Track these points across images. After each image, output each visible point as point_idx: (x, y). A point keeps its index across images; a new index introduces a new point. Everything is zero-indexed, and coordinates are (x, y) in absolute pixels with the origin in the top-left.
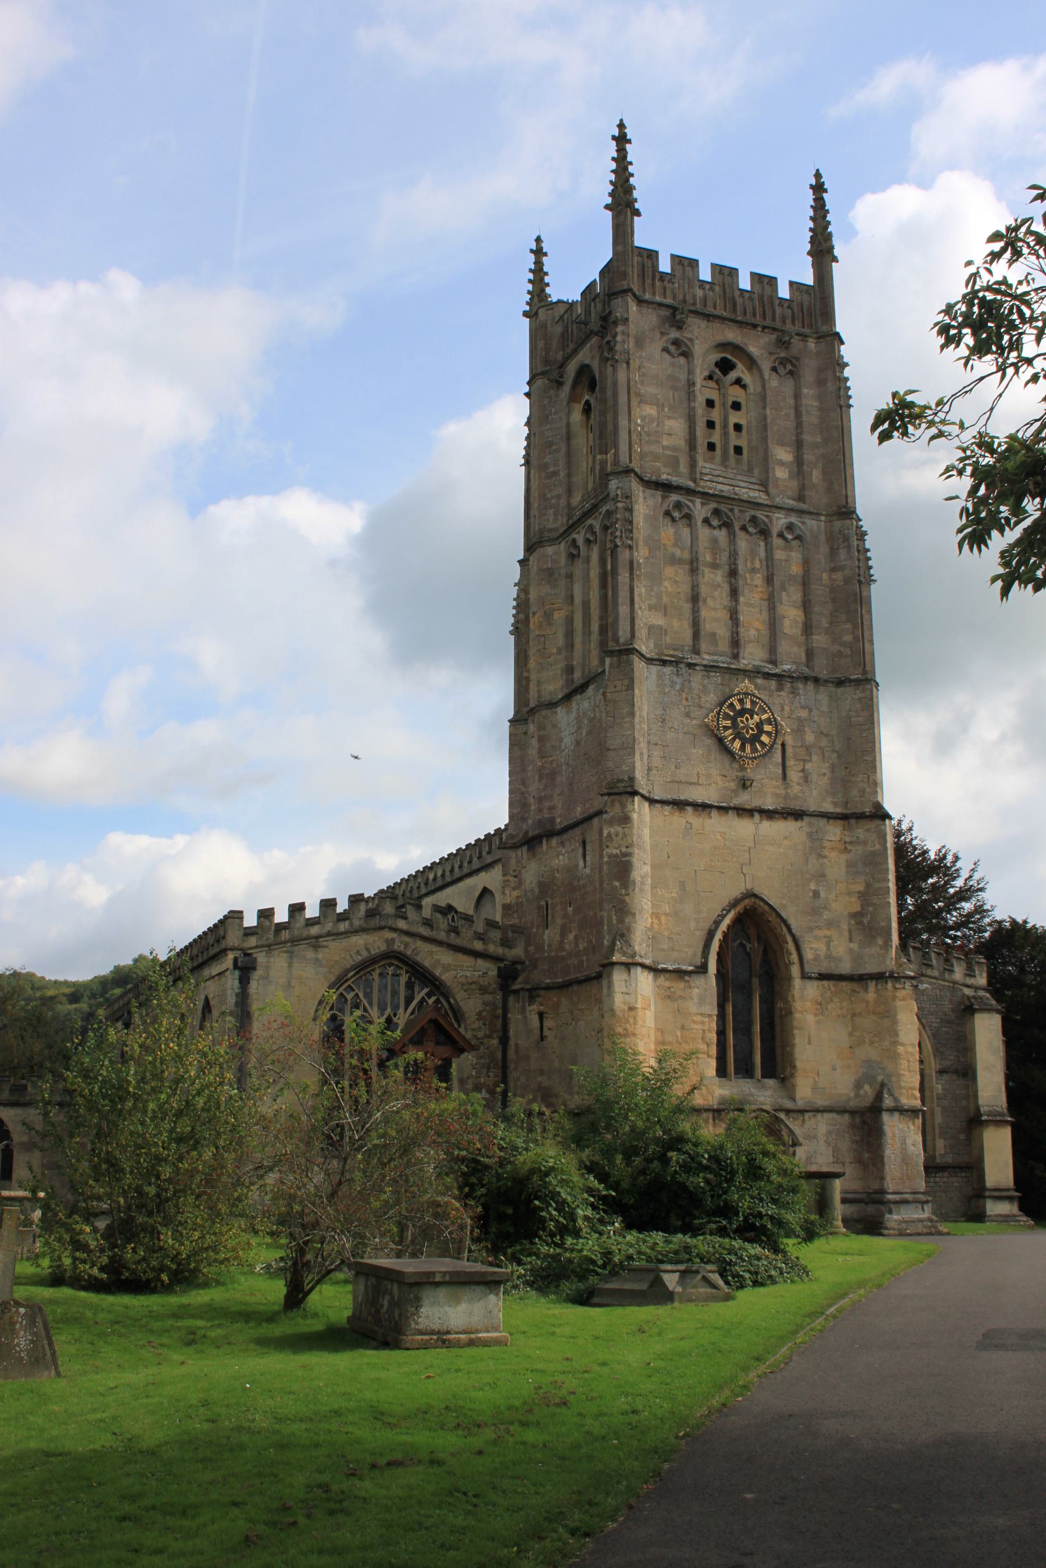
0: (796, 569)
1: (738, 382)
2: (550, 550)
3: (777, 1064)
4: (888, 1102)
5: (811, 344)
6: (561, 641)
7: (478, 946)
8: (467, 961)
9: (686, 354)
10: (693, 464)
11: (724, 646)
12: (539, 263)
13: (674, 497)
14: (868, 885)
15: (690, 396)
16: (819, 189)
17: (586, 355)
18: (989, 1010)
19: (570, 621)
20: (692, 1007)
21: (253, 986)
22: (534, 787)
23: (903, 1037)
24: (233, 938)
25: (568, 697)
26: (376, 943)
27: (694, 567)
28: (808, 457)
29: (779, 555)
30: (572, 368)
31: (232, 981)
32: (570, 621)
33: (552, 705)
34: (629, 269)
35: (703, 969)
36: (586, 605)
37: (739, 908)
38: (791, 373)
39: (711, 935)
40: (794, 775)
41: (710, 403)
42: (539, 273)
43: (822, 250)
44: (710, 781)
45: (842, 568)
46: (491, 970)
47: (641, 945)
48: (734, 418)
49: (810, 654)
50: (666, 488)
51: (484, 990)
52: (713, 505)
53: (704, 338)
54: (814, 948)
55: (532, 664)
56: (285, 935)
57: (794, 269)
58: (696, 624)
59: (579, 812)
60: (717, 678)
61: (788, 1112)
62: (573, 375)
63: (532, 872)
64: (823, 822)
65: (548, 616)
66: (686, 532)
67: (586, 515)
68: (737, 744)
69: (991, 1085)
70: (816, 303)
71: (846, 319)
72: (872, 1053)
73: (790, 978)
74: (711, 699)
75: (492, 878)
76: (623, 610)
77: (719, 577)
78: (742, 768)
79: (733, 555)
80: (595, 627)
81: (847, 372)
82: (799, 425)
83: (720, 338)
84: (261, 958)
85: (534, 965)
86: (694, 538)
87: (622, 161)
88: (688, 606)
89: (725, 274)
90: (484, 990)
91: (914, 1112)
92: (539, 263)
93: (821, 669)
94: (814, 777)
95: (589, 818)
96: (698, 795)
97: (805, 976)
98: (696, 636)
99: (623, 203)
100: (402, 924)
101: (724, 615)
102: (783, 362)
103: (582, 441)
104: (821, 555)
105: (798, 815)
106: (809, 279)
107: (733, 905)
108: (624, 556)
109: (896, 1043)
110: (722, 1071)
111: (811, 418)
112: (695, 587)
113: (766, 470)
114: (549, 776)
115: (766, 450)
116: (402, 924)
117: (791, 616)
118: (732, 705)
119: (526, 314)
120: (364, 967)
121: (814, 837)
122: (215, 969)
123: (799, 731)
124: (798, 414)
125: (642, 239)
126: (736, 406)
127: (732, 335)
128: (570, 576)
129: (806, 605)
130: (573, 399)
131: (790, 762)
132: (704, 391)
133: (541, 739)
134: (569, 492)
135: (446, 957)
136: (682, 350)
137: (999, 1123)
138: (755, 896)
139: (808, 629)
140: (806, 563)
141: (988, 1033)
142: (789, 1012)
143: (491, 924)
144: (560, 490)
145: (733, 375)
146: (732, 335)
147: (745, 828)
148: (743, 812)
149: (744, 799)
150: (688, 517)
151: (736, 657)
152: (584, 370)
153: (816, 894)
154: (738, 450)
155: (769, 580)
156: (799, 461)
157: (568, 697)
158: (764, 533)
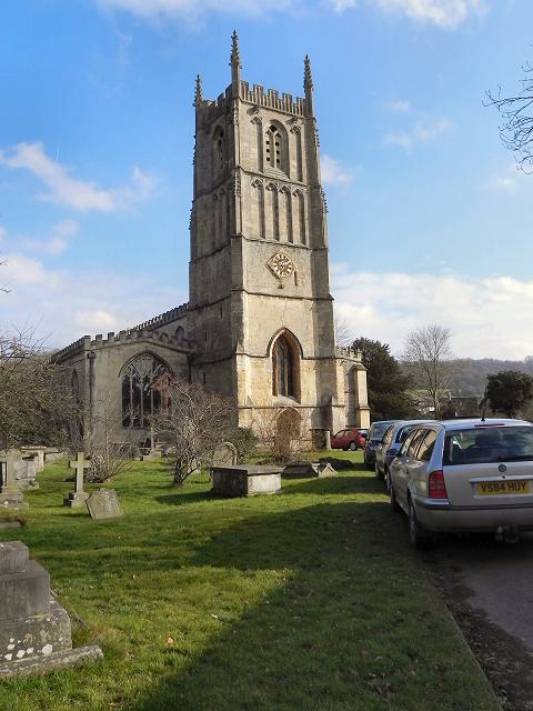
2: (205, 197)
4: (333, 403)
6: (210, 232)
7: (180, 348)
8: (176, 354)
13: (255, 178)
16: (307, 62)
17: (218, 122)
19: (214, 224)
20: (264, 369)
21: (95, 365)
22: (200, 288)
24: (87, 346)
25: (213, 254)
26: (141, 347)
30: (214, 126)
31: (87, 362)
32: (214, 224)
33: (207, 256)
35: (268, 355)
36: (220, 218)
42: (198, 88)
43: (308, 86)
44: (270, 286)
46: (184, 357)
47: (247, 349)
51: (182, 365)
55: (199, 241)
56: (106, 345)
59: (219, 297)
60: (271, 247)
63: (200, 321)
65: (205, 222)
67: (220, 184)
69: (363, 398)
72: (328, 386)
75: (182, 323)
80: (225, 227)
83: (272, 118)
84: (98, 354)
85: (201, 355)
90: (182, 365)
95: (223, 299)
96: (265, 291)
99: (235, 63)
100: (151, 340)
103: (218, 156)
105: (301, 299)
107: (278, 332)
110: (274, 394)
114: (206, 284)
116: (151, 340)
120: (138, 356)
122: (78, 358)
125: (204, 98)
127: (276, 116)
128: (213, 208)
130: (214, 139)
133: (203, 270)
134: (213, 174)
135: (167, 352)
136: (258, 122)
141: (362, 376)
142: (299, 371)
143: (183, 339)
144: (210, 174)
146: (276, 116)
147: (282, 302)
149: (281, 292)
152: (218, 127)
157: (213, 254)
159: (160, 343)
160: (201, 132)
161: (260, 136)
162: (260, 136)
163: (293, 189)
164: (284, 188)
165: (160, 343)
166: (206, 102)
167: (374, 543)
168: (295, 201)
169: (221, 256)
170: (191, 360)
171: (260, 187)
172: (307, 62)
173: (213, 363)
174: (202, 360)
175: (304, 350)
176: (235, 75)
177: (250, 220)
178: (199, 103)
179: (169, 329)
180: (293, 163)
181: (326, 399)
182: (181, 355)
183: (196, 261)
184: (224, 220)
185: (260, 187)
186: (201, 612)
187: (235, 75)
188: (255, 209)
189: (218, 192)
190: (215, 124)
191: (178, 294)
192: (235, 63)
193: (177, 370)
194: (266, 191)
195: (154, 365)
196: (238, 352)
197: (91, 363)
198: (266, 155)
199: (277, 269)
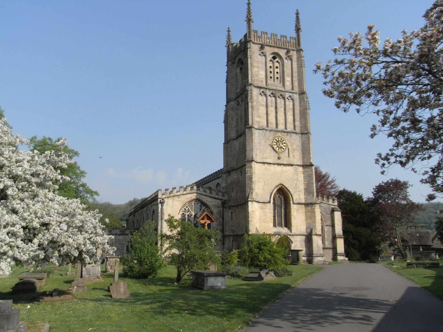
1: (277, 62)
3: (288, 224)
8: (214, 200)
13: (262, 90)
16: (297, 14)
24: (160, 196)
30: (237, 59)
37: (278, 187)
39: (272, 194)
40: (291, 156)
42: (229, 36)
43: (298, 30)
44: (271, 157)
45: (302, 106)
46: (220, 202)
48: (276, 70)
51: (218, 207)
56: (172, 195)
60: (272, 132)
61: (290, 235)
64: (298, 167)
65: (232, 118)
68: (277, 148)
69: (339, 229)
73: (290, 204)
74: (271, 138)
80: (243, 121)
84: (166, 200)
87: (298, 18)
90: (218, 207)
91: (320, 235)
96: (268, 161)
97: (293, 203)
99: (249, 21)
103: (240, 77)
105: (292, 165)
107: (277, 187)
109: (315, 219)
110: (275, 225)
118: (276, 140)
122: (155, 203)
126: (277, 67)
127: (276, 50)
131: (290, 153)
132: (269, 64)
134: (237, 88)
138: (282, 185)
141: (338, 216)
148: (278, 164)
151: (277, 128)
153: (296, 184)
154: (277, 78)
159: (204, 193)
160: (230, 63)
161: (266, 63)
162: (266, 63)
163: (287, 95)
164: (281, 95)
165: (204, 193)
166: (232, 44)
167: (34, 220)
168: (289, 104)
169: (241, 139)
170: (224, 204)
171: (265, 95)
172: (297, 14)
173: (237, 206)
174: (231, 204)
175: (294, 198)
176: (249, 27)
177: (259, 117)
178: (229, 44)
179: (212, 185)
180: (288, 79)
181: (309, 230)
182: (218, 201)
183: (227, 142)
184: (243, 116)
185: (265, 95)
186: (35, 216)
187: (249, 27)
188: (263, 110)
189: (240, 100)
190: (238, 58)
191: (216, 163)
192: (249, 21)
193: (215, 210)
194: (269, 98)
195: (201, 206)
196: (249, 199)
197: (162, 206)
198: (269, 75)
199: (277, 146)
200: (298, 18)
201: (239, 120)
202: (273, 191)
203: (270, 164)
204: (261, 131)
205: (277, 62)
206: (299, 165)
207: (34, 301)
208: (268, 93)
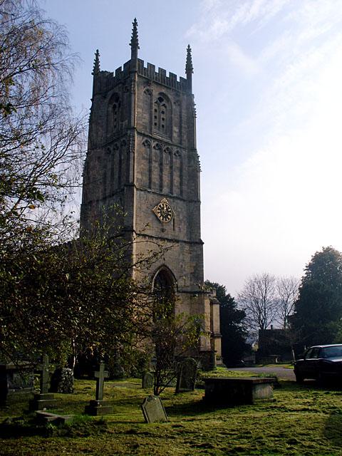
0: (178, 165)
1: (164, 105)
5: (185, 97)
9: (151, 94)
10: (151, 129)
11: (157, 187)
12: (97, 58)
13: (146, 138)
14: (197, 264)
15: (151, 107)
16: (135, 24)
18: (217, 304)
23: (206, 311)
27: (150, 162)
28: (183, 131)
29: (174, 160)
30: (110, 93)
34: (133, 65)
37: (161, 269)
38: (179, 105)
40: (177, 229)
41: (156, 110)
42: (97, 62)
43: (189, 69)
45: (192, 166)
48: (162, 116)
49: (181, 192)
50: (144, 135)
52: (156, 143)
53: (156, 92)
54: (180, 283)
57: (181, 74)
58: (150, 179)
62: (110, 96)
64: (184, 244)
66: (148, 149)
68: (161, 218)
70: (187, 83)
71: (196, 89)
76: (131, 172)
77: (157, 165)
78: (163, 226)
79: (162, 158)
81: (195, 107)
82: (181, 121)
86: (151, 152)
87: (135, 31)
88: (148, 173)
89: (163, 71)
92: (97, 58)
93: (185, 197)
94: (182, 230)
98: (150, 183)
99: (134, 44)
101: (158, 177)
102: (177, 101)
104: (185, 161)
105: (177, 241)
106: (185, 77)
107: (159, 268)
108: (132, 154)
109: (204, 313)
111: (184, 119)
112: (150, 167)
113: (172, 133)
115: (172, 127)
117: (176, 179)
118: (160, 206)
119: (92, 74)
121: (182, 248)
123: (178, 215)
124: (181, 117)
126: (163, 112)
127: (163, 91)
129: (181, 176)
130: (110, 102)
131: (176, 225)
132: (154, 107)
136: (149, 92)
137: (218, 337)
138: (166, 266)
139: (181, 184)
140: (181, 163)
145: (163, 103)
149: (163, 235)
150: (149, 145)
151: (161, 190)
153: (182, 266)
154: (163, 126)
155: (171, 167)
156: (180, 132)
158: (170, 153)
163: (175, 150)
172: (135, 24)
178: (97, 73)
192: (134, 44)
200: (135, 31)
201: (109, 174)
202: (154, 274)
203: (152, 237)
204: (142, 193)
205: (164, 105)
206: (185, 242)
207: (37, 435)
208: (153, 144)
